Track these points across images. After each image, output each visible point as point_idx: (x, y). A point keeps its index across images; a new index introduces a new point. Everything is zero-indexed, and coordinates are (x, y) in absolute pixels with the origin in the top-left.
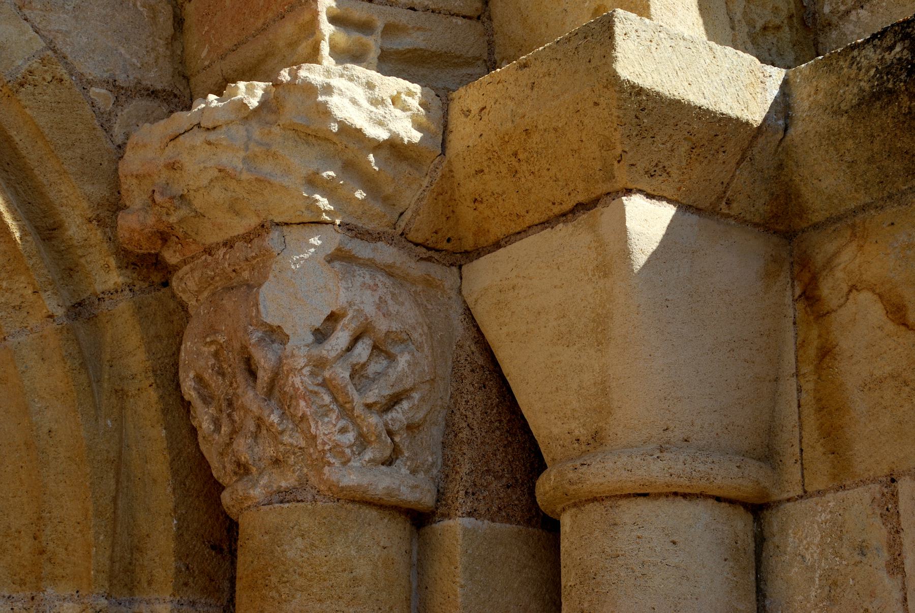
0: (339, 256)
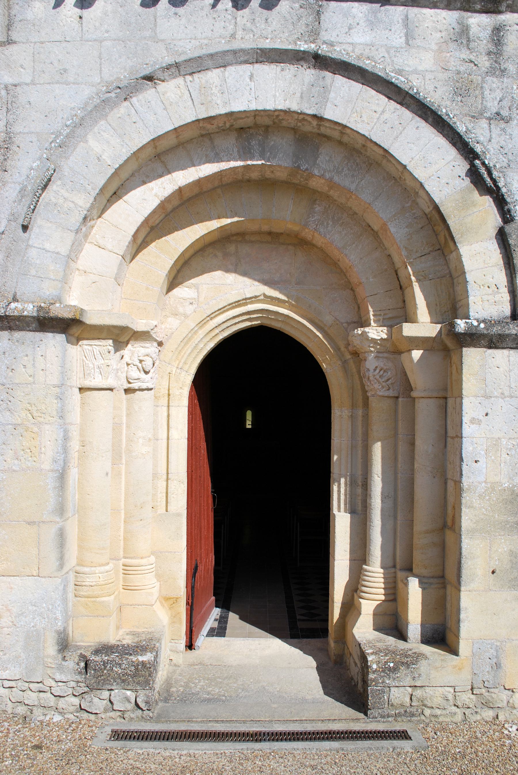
0: (376, 357)
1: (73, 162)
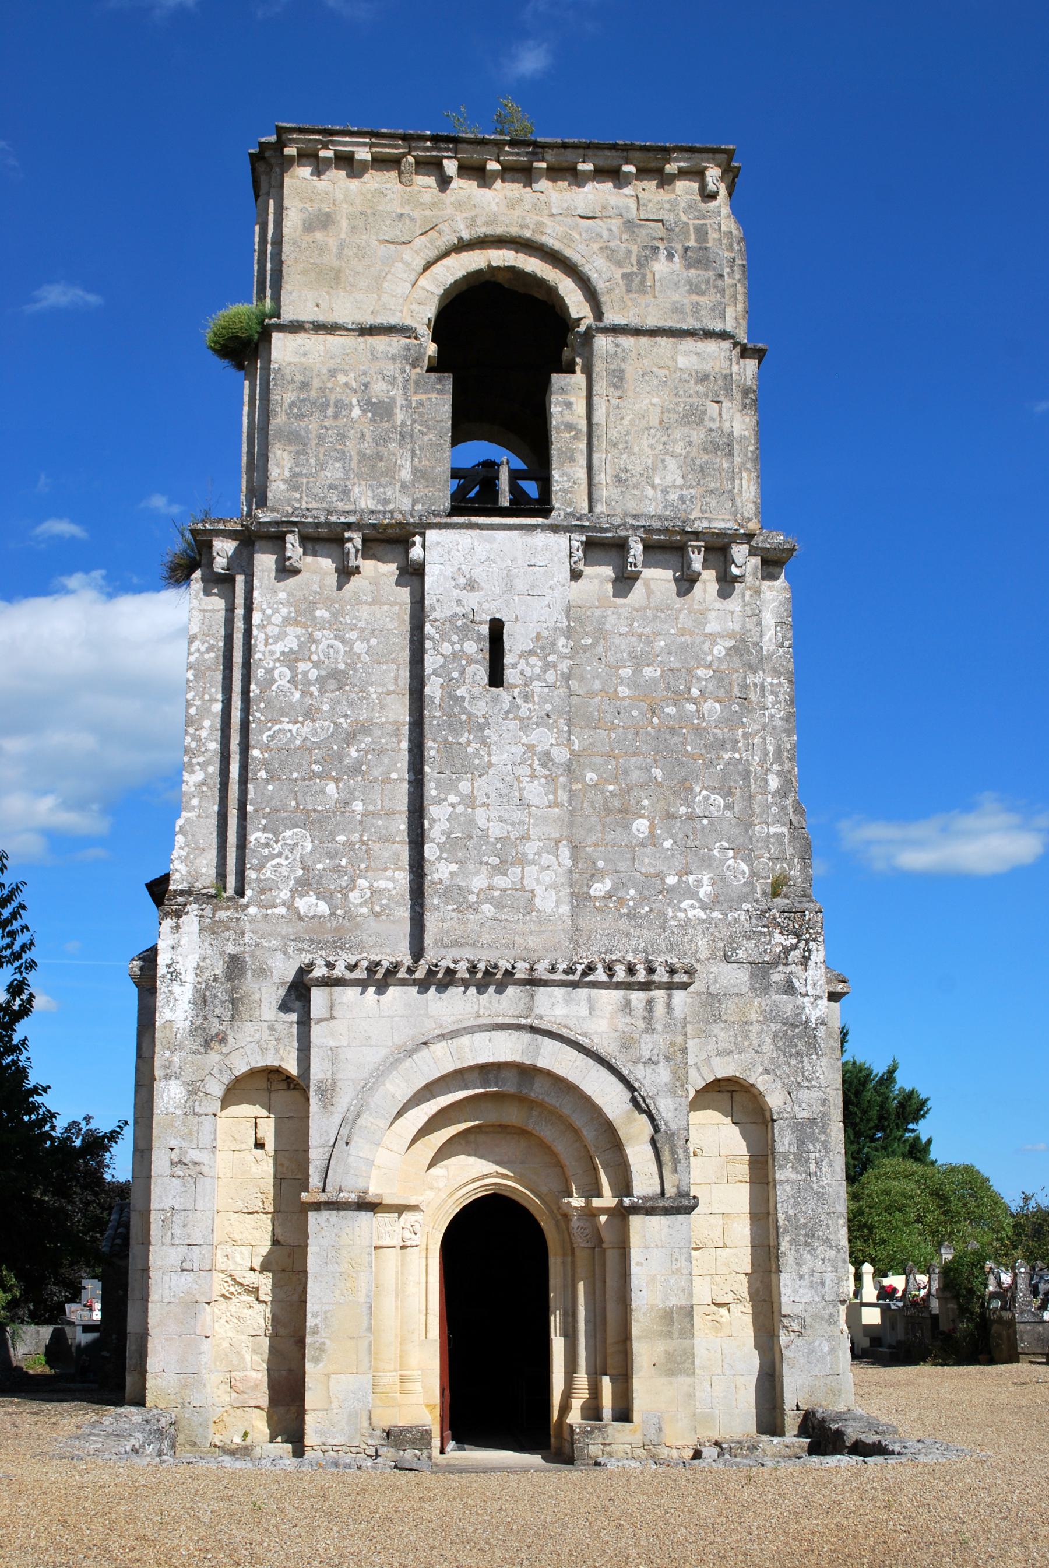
1: (376, 1099)
